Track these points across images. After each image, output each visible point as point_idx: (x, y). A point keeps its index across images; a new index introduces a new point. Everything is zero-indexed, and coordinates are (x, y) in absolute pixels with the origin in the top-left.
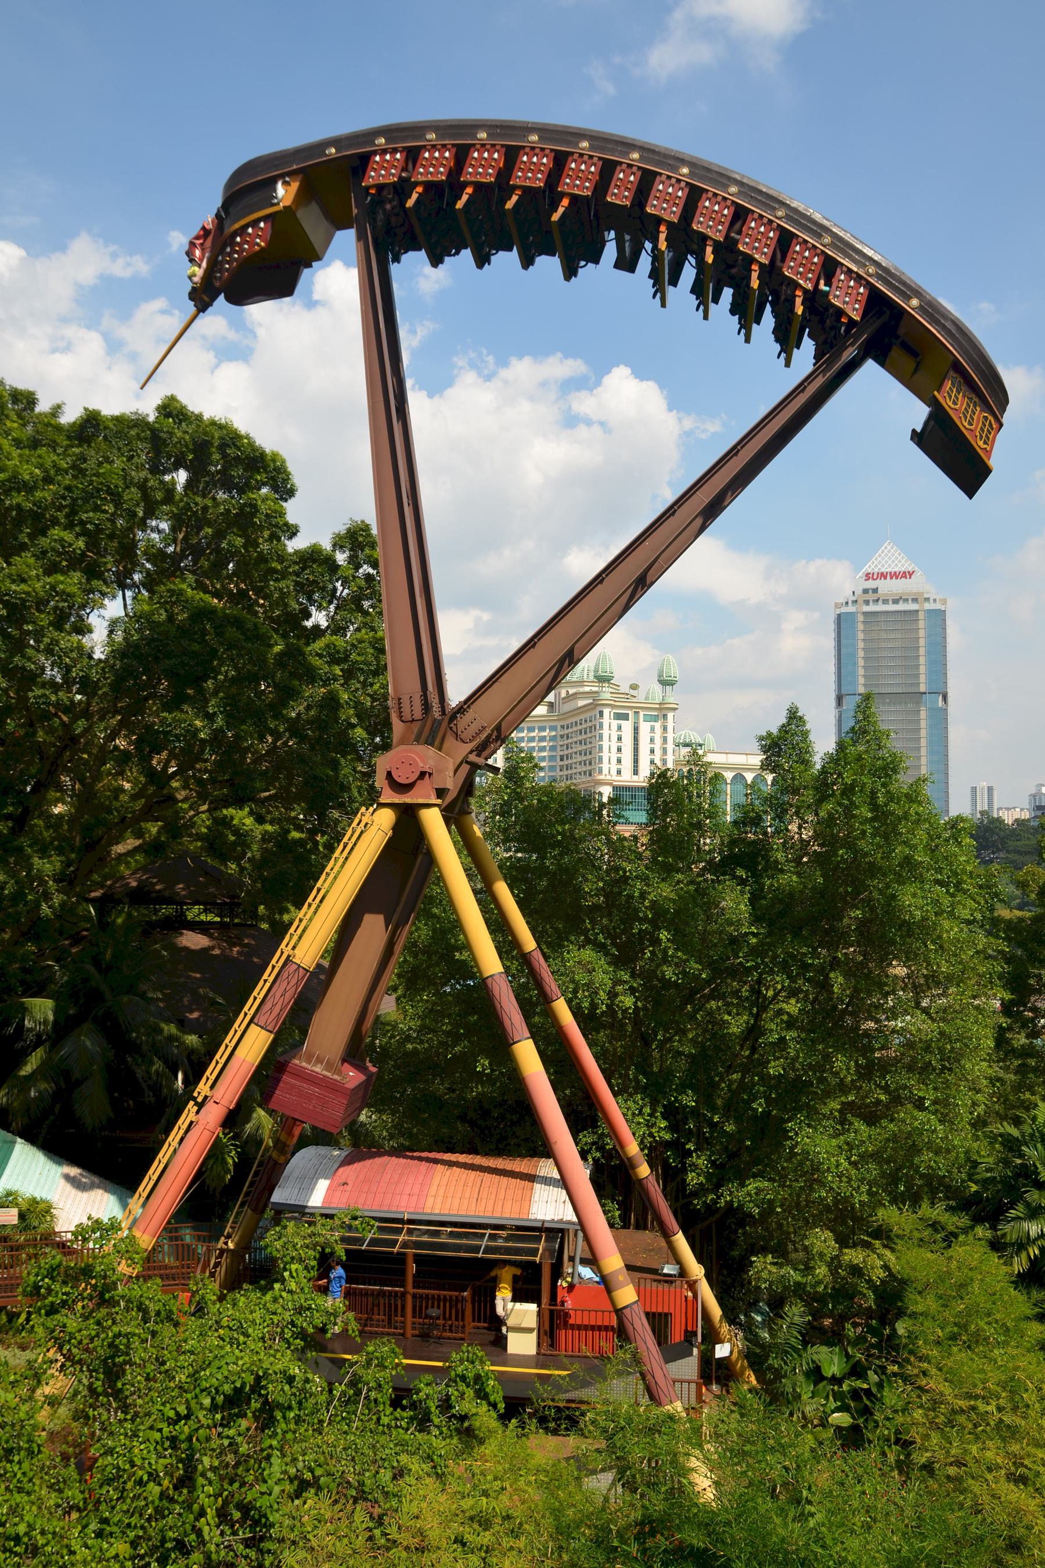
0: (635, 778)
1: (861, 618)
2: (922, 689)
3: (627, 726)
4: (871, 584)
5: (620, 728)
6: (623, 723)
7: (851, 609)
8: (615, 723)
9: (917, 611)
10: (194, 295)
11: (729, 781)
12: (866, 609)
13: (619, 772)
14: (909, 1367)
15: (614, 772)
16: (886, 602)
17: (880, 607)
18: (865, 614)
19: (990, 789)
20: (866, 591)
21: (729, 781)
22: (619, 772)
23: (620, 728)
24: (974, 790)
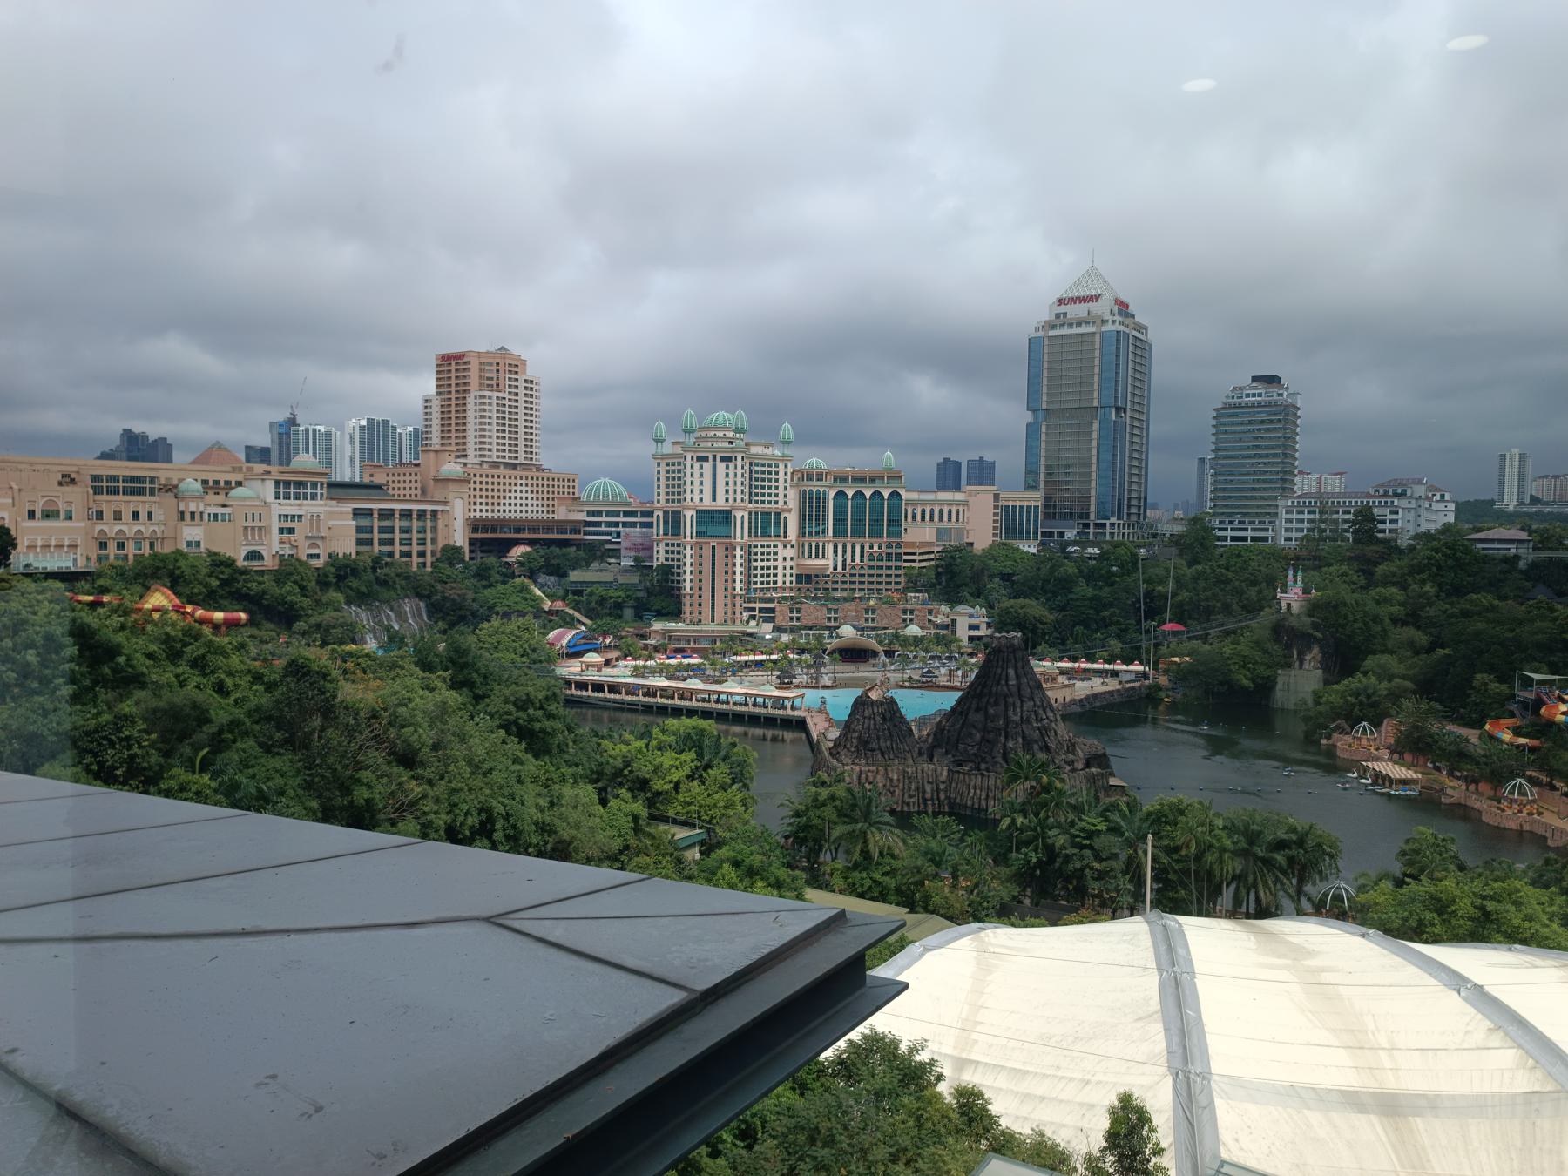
0: (714, 503)
1: (1046, 342)
2: (1096, 404)
3: (708, 466)
4: (1062, 309)
5: (701, 467)
6: (705, 464)
7: (1041, 334)
8: (697, 465)
9: (1094, 333)
10: (102, 453)
11: (868, 497)
12: (1052, 333)
13: (701, 500)
14: (1294, 881)
15: (696, 499)
16: (1071, 325)
17: (1066, 331)
18: (1050, 338)
19: (1522, 457)
20: (1058, 315)
21: (868, 497)
22: (701, 500)
23: (701, 467)
24: (1503, 457)
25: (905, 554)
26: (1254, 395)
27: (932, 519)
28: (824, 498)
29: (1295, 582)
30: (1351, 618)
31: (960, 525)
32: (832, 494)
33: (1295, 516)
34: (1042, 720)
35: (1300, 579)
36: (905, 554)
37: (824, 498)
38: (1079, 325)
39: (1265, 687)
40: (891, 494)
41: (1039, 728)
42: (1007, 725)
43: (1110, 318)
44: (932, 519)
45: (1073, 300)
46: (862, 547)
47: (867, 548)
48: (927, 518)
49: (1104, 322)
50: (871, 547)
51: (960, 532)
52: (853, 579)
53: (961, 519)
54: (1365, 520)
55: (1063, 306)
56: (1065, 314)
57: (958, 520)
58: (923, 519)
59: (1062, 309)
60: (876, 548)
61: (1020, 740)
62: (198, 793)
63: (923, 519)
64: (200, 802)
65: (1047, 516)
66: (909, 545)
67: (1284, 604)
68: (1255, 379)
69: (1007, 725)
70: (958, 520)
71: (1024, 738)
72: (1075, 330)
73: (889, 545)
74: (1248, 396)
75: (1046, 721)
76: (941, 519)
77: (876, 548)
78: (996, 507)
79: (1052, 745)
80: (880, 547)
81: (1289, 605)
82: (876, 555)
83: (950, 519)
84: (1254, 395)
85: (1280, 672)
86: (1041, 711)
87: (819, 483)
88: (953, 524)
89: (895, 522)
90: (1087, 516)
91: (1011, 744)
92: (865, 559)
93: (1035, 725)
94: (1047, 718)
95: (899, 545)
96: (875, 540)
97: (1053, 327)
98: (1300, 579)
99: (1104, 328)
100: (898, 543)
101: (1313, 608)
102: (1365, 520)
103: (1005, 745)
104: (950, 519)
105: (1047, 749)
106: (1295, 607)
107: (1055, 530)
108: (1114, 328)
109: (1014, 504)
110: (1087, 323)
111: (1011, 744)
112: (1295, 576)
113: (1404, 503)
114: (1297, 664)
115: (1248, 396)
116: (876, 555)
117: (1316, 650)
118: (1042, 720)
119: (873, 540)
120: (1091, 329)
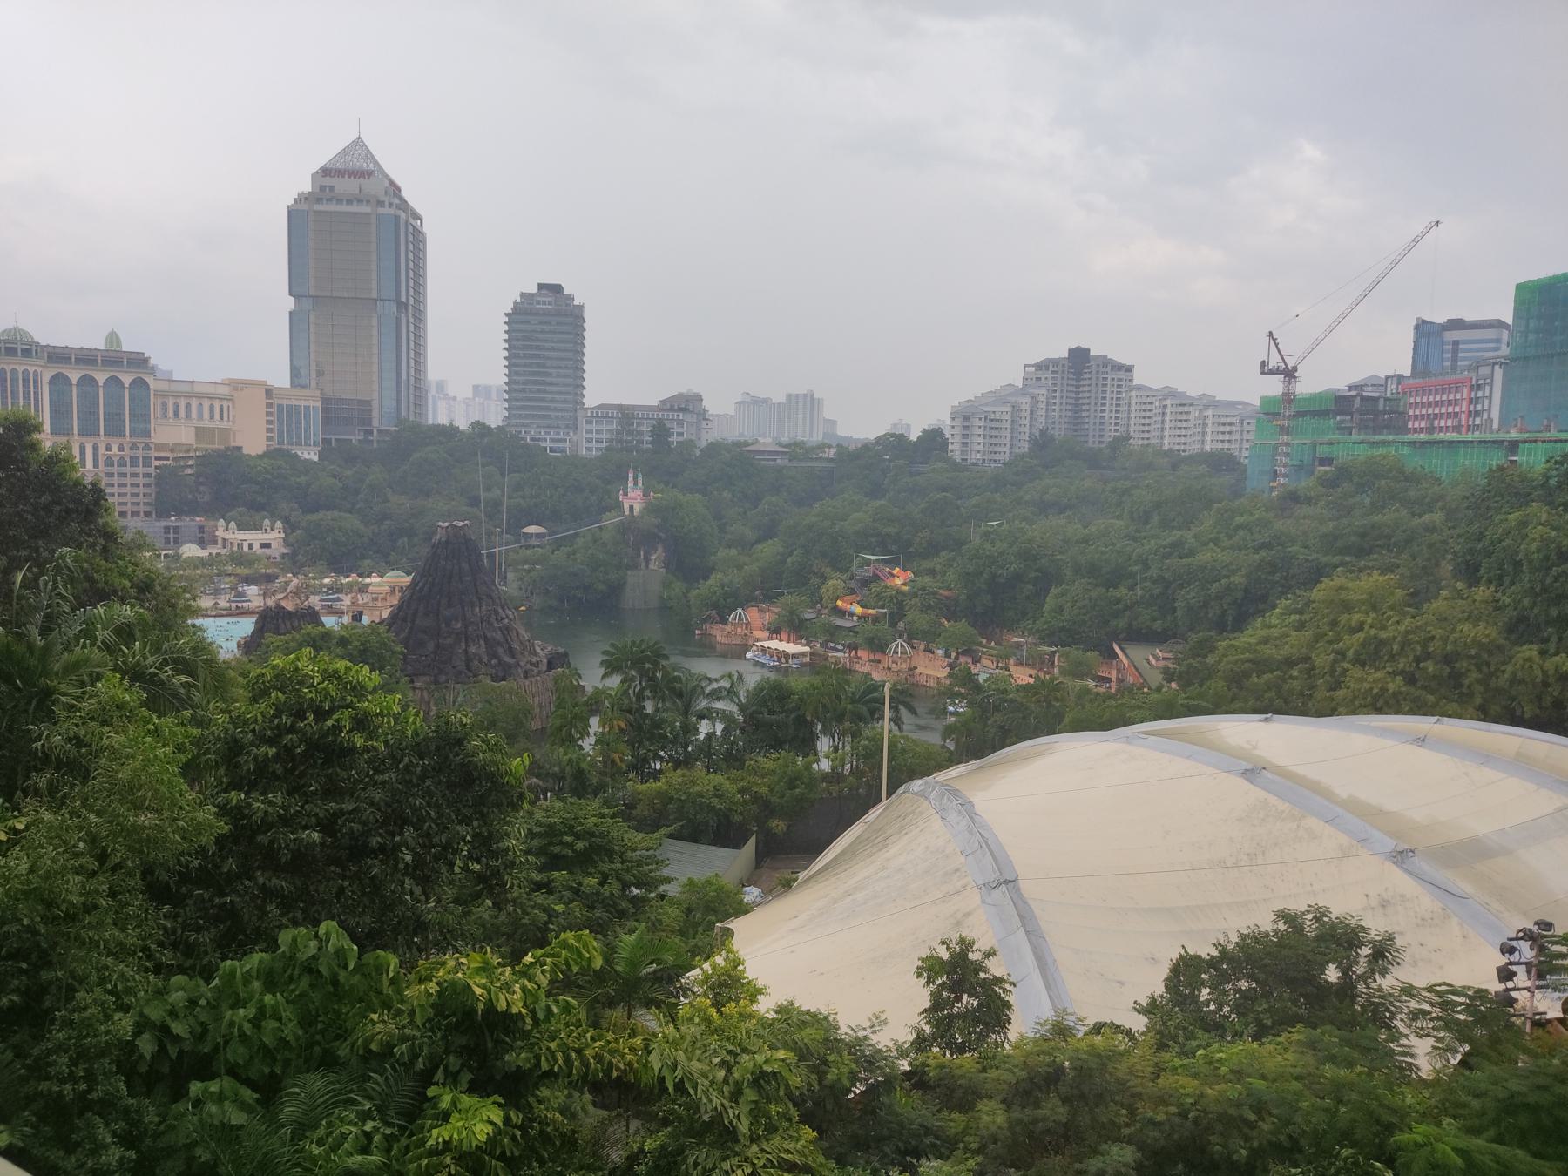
2: (374, 295)
4: (328, 181)
7: (304, 206)
11: (101, 384)
12: (318, 207)
16: (339, 201)
17: (333, 207)
20: (323, 188)
21: (101, 384)
25: (157, 459)
26: (544, 303)
27: (188, 416)
28: (36, 382)
29: (636, 484)
30: (687, 519)
31: (225, 425)
32: (47, 376)
33: (594, 426)
34: (503, 619)
35: (640, 480)
36: (157, 459)
37: (36, 382)
38: (349, 202)
39: (616, 589)
40: (133, 382)
41: (500, 628)
42: (466, 627)
43: (386, 199)
44: (188, 416)
45: (340, 173)
46: (95, 448)
47: (102, 450)
48: (182, 413)
49: (380, 203)
50: (108, 448)
51: (225, 433)
52: (123, 481)
53: (225, 418)
54: (661, 432)
55: (328, 178)
56: (332, 188)
57: (222, 418)
58: (177, 414)
59: (328, 181)
60: (115, 449)
61: (482, 642)
62: (1237, 679)
63: (177, 414)
64: (404, 205)
65: (326, 421)
66: (159, 447)
67: (626, 507)
68: (541, 286)
69: (466, 627)
70: (222, 418)
71: (486, 639)
72: (344, 208)
73: (134, 447)
74: (538, 303)
75: (506, 621)
76: (200, 417)
77: (115, 449)
78: (269, 405)
79: (516, 646)
80: (121, 449)
81: (631, 508)
82: (116, 459)
83: (212, 417)
84: (544, 303)
85: (629, 572)
86: (500, 611)
87: (26, 361)
88: (217, 424)
89: (141, 416)
90: (370, 423)
91: (473, 649)
92: (101, 464)
93: (496, 625)
94: (507, 617)
95: (147, 447)
96: (115, 439)
97: (319, 200)
98: (640, 480)
99: (380, 210)
100: (147, 445)
101: (650, 508)
102: (661, 432)
103: (466, 651)
104: (212, 417)
105: (511, 652)
106: (637, 508)
107: (333, 437)
108: (392, 211)
109: (289, 403)
110: (360, 201)
111: (473, 649)
112: (635, 478)
113: (688, 417)
114: (643, 564)
115: (538, 303)
116: (116, 459)
117: (660, 550)
118: (503, 619)
119: (110, 440)
120: (365, 209)
